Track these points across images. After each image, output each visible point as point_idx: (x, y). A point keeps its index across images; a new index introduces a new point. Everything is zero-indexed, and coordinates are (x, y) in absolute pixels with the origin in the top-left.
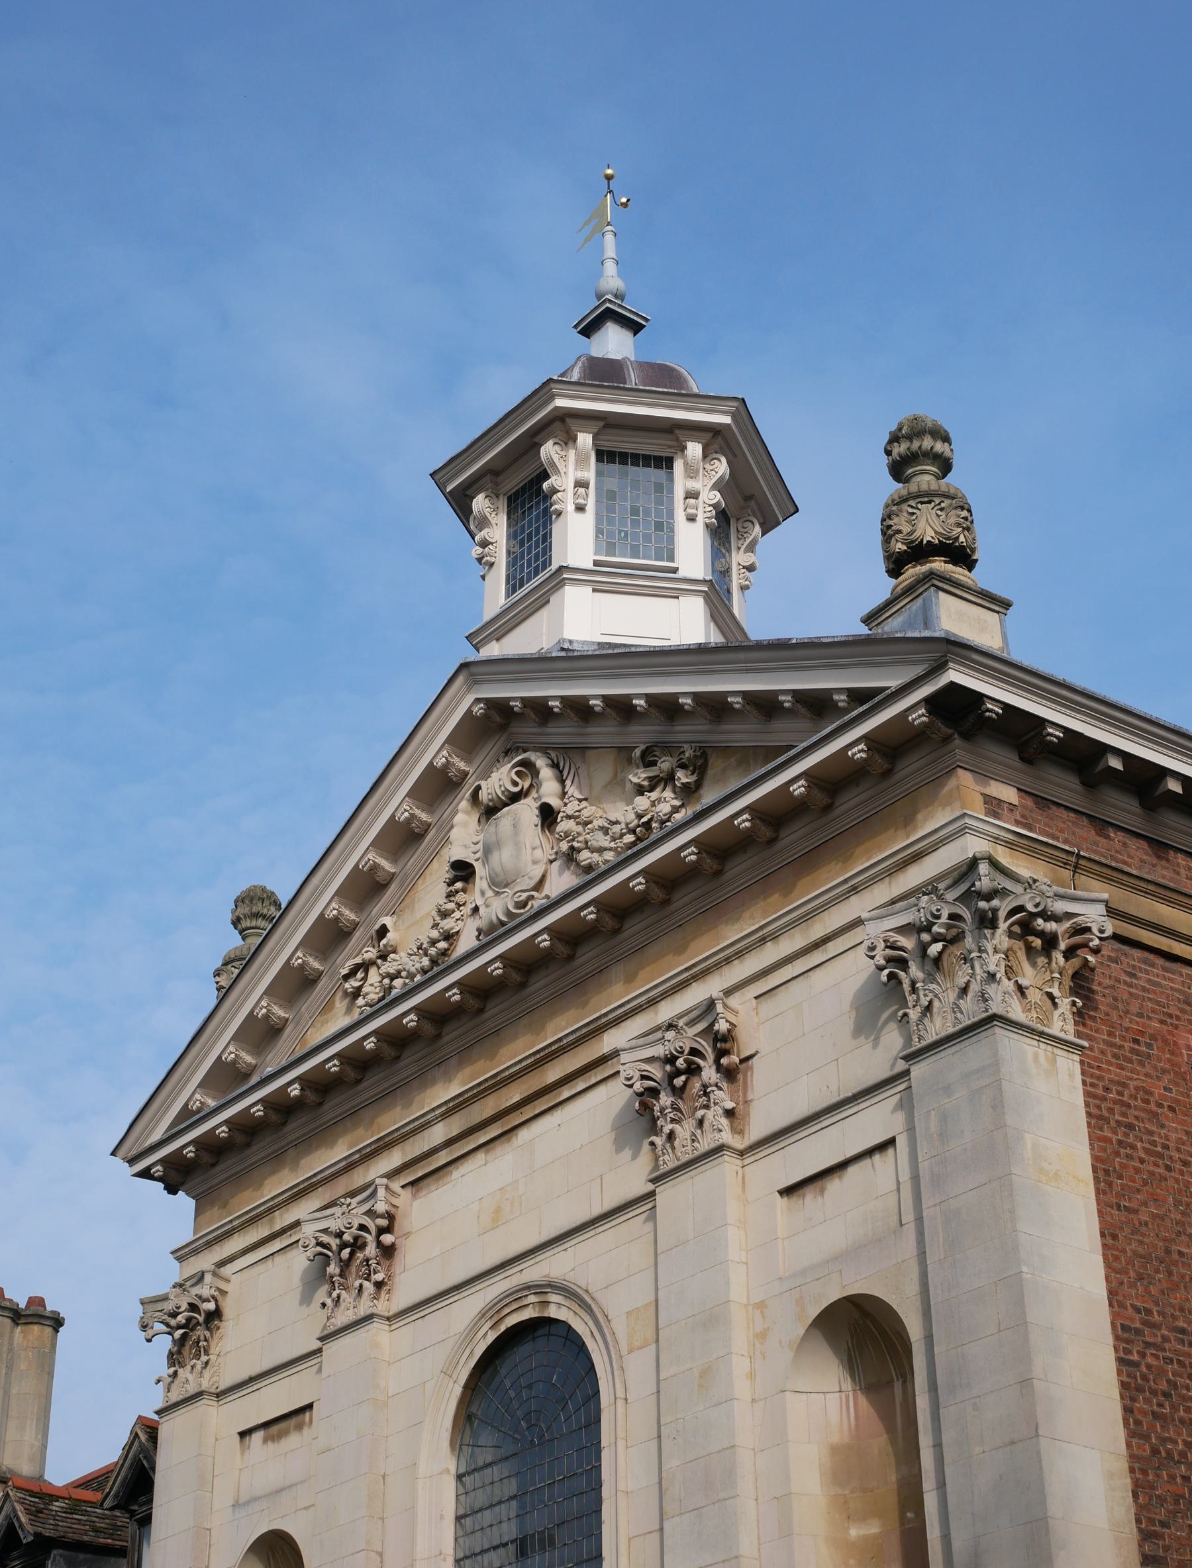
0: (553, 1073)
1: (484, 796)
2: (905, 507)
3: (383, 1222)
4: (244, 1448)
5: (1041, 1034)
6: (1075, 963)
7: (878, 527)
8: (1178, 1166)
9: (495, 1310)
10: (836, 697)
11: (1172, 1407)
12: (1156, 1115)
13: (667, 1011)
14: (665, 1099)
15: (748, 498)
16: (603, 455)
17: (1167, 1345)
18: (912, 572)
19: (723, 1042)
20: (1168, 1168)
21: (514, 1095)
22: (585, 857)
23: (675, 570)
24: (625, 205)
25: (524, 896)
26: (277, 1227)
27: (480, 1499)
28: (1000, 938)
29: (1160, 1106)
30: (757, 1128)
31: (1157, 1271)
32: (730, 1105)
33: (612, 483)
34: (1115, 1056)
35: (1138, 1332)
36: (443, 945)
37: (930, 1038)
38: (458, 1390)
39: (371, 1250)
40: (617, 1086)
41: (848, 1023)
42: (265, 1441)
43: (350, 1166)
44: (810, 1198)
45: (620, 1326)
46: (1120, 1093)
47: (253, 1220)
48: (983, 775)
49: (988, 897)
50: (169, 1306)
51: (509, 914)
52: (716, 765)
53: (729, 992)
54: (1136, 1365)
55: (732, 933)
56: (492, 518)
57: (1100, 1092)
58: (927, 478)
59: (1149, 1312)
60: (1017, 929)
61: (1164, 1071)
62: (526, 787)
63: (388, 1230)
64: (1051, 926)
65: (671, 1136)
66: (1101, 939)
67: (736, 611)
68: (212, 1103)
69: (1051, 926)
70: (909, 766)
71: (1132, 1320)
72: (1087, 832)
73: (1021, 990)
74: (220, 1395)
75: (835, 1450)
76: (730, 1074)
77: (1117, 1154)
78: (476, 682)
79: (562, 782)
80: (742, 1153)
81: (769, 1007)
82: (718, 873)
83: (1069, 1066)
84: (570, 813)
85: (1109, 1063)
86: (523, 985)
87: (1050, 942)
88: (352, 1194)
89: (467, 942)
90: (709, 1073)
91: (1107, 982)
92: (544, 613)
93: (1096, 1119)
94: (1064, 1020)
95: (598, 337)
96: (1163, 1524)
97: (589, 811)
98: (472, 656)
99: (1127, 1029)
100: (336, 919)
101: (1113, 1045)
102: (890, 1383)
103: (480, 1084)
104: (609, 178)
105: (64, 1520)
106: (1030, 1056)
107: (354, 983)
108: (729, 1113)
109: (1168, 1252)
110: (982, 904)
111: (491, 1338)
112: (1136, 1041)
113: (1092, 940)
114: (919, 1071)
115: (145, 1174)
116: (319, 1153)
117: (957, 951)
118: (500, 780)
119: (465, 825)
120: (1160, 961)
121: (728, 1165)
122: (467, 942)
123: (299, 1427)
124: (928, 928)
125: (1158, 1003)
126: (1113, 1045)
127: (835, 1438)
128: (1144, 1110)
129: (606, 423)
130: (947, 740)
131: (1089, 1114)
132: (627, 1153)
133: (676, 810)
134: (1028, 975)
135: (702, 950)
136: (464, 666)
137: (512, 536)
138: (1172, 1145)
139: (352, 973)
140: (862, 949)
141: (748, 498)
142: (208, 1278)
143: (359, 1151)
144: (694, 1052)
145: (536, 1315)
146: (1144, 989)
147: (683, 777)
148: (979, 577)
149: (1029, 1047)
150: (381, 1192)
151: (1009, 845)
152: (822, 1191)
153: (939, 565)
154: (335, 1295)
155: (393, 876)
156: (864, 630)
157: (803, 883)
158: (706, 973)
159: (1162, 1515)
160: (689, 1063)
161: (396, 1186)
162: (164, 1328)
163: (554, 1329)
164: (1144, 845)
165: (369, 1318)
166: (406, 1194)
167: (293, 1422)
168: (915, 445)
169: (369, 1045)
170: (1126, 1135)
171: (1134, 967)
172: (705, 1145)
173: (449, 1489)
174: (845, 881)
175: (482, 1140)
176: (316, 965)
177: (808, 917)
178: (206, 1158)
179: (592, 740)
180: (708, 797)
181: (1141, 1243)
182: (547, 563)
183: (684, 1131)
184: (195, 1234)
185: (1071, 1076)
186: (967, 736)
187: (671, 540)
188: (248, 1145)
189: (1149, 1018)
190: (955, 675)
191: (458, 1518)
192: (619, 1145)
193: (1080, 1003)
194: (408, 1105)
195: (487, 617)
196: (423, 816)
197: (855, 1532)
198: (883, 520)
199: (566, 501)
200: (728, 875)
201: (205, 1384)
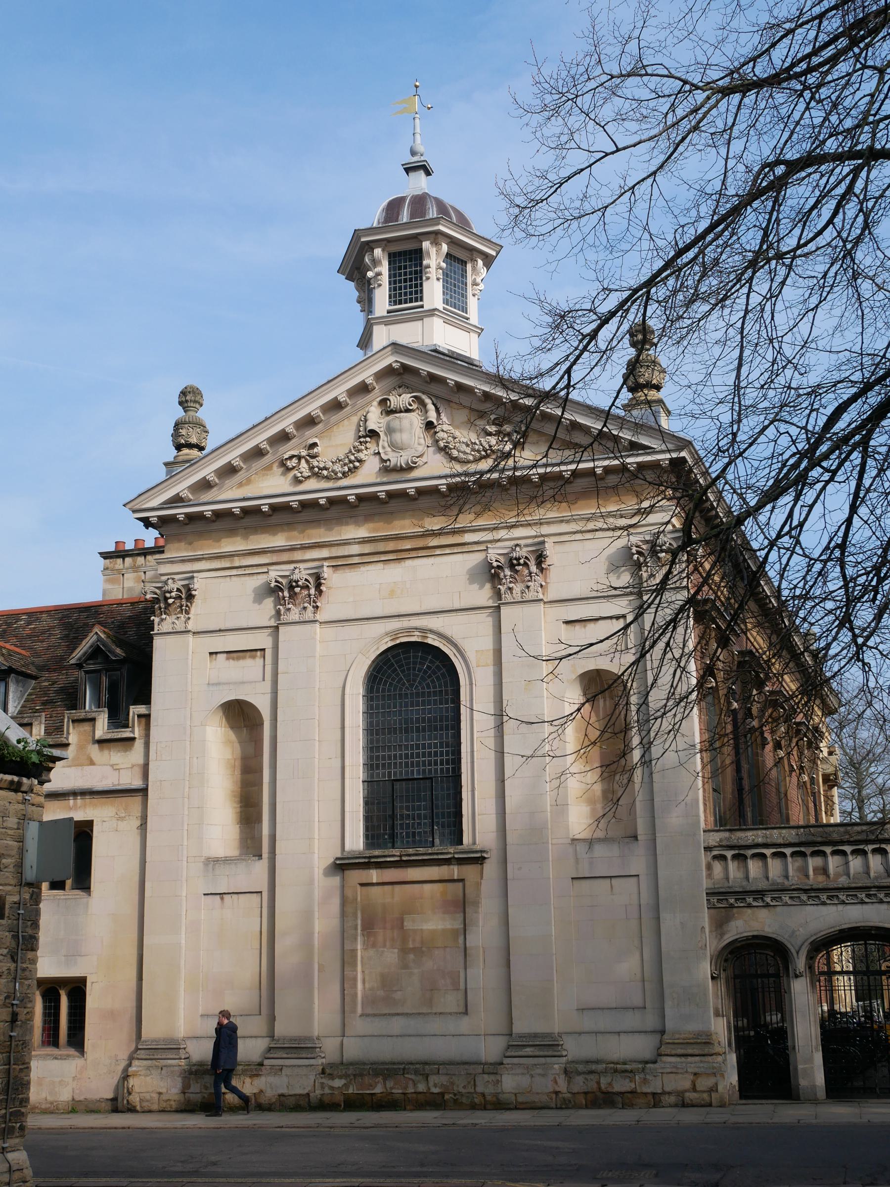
9: (395, 634)
19: (540, 558)
23: (468, 319)
78: (397, 352)
81: (559, 548)
116: (263, 536)
129: (453, 242)
145: (419, 640)
147: (515, 437)
152: (585, 627)
167: (248, 654)
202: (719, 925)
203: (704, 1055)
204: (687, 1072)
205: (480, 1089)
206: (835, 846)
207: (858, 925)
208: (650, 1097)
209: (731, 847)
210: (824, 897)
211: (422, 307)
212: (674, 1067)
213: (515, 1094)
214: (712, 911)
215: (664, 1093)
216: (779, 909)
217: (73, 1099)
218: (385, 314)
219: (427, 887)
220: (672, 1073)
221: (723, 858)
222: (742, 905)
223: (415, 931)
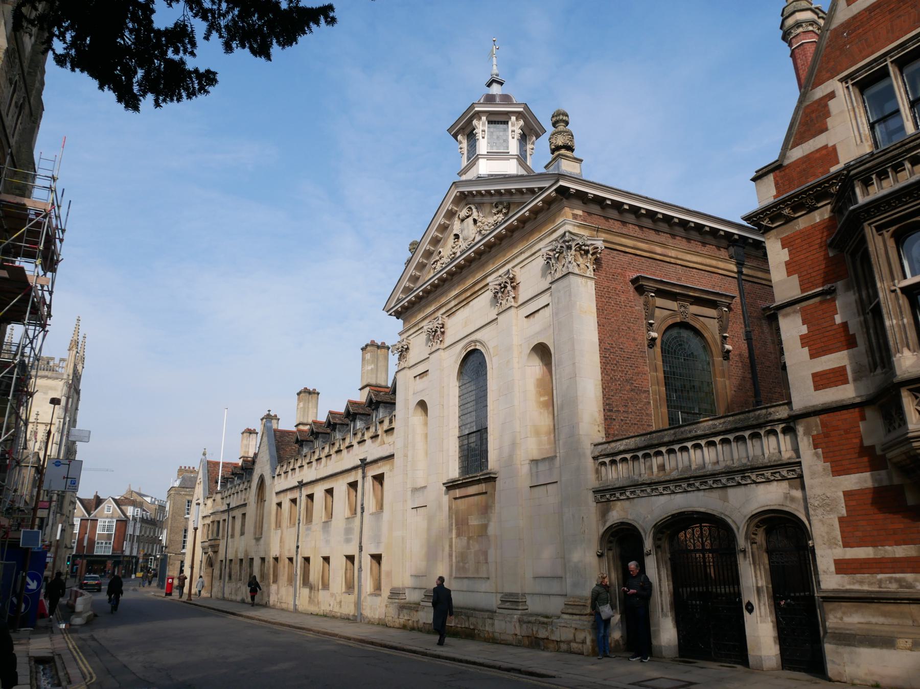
0: (477, 288)
1: (460, 217)
3: (441, 326)
4: (415, 380)
6: (595, 256)
9: (465, 347)
11: (617, 367)
12: (618, 294)
13: (501, 272)
14: (500, 294)
15: (532, 130)
16: (490, 122)
18: (556, 153)
19: (512, 280)
20: (620, 308)
21: (468, 294)
22: (483, 232)
23: (508, 153)
24: (498, 49)
27: (465, 391)
28: (573, 252)
30: (520, 302)
32: (514, 296)
33: (492, 130)
35: (608, 349)
36: (453, 256)
37: (556, 278)
38: (458, 366)
39: (439, 333)
41: (540, 275)
42: (420, 378)
43: (434, 312)
44: (531, 318)
45: (491, 350)
47: (415, 326)
48: (572, 208)
49: (568, 242)
50: (397, 347)
51: (467, 248)
53: (514, 267)
55: (515, 251)
56: (463, 141)
58: (562, 127)
59: (612, 344)
60: (578, 249)
61: (621, 282)
63: (443, 327)
64: (587, 248)
65: (501, 304)
67: (528, 164)
68: (404, 297)
69: (587, 248)
70: (554, 207)
72: (603, 221)
73: (578, 265)
74: (409, 368)
75: (538, 380)
76: (514, 288)
77: (606, 305)
79: (478, 212)
80: (517, 308)
81: (524, 270)
82: (512, 236)
83: (591, 285)
86: (470, 266)
87: (587, 252)
88: (434, 319)
89: (458, 254)
90: (509, 288)
92: (475, 166)
95: (491, 87)
96: (612, 396)
97: (484, 220)
98: (457, 179)
100: (429, 250)
104: (494, 41)
106: (580, 282)
107: (434, 266)
108: (514, 298)
109: (619, 329)
110: (567, 244)
112: (613, 275)
114: (553, 286)
115: (390, 315)
117: (562, 255)
118: (464, 213)
119: (457, 224)
120: (622, 254)
121: (513, 311)
123: (426, 375)
124: (555, 250)
129: (490, 113)
130: (562, 199)
132: (493, 308)
133: (503, 219)
134: (581, 261)
135: (509, 256)
136: (454, 183)
137: (468, 145)
140: (541, 257)
141: (532, 130)
142: (405, 340)
144: (506, 282)
147: (504, 211)
148: (576, 154)
149: (579, 279)
150: (440, 318)
153: (563, 151)
155: (442, 238)
156: (544, 171)
157: (531, 238)
159: (612, 393)
160: (505, 285)
161: (444, 317)
164: (619, 223)
165: (439, 349)
166: (447, 318)
168: (558, 118)
169: (436, 282)
172: (508, 306)
173: (457, 389)
176: (425, 261)
177: (531, 247)
178: (404, 310)
179: (485, 201)
180: (510, 215)
182: (475, 153)
183: (504, 302)
185: (592, 286)
186: (567, 199)
188: (413, 307)
190: (562, 183)
191: (459, 397)
192: (491, 305)
194: (447, 297)
195: (462, 168)
196: (448, 222)
197: (542, 399)
199: (479, 136)
200: (514, 236)
201: (406, 366)
202: (604, 514)
203: (582, 615)
204: (571, 627)
207: (683, 510)
209: (607, 455)
210: (661, 489)
212: (566, 623)
214: (599, 505)
215: (561, 641)
216: (636, 500)
218: (486, 153)
220: (564, 627)
221: (604, 464)
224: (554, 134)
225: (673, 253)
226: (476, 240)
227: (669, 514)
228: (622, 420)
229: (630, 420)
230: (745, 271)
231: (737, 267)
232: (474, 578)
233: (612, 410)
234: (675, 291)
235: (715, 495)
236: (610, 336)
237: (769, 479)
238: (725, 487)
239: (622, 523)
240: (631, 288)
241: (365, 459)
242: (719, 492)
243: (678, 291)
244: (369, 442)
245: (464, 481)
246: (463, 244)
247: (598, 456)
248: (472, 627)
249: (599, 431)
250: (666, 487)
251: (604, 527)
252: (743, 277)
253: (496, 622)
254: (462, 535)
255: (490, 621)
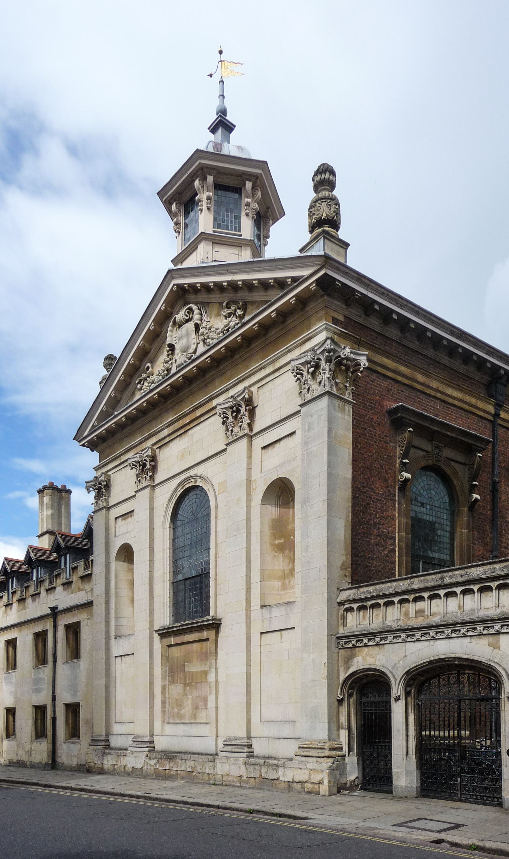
0: (198, 413)
2: (317, 204)
5: (341, 398)
7: (307, 212)
8: (378, 441)
10: (288, 280)
17: (367, 493)
19: (249, 402)
20: (375, 442)
21: (187, 420)
25: (190, 355)
26: (122, 461)
29: (376, 423)
31: (367, 472)
34: (364, 407)
35: (359, 488)
40: (216, 417)
42: (122, 520)
46: (364, 419)
52: (250, 308)
54: (358, 497)
57: (358, 418)
59: (363, 483)
62: (190, 317)
66: (363, 368)
71: (358, 485)
83: (349, 409)
84: (204, 326)
85: (361, 409)
87: (348, 368)
91: (364, 383)
93: (355, 426)
94: (349, 394)
99: (369, 398)
101: (363, 403)
102: (289, 503)
103: (177, 417)
105: (73, 542)
111: (181, 491)
112: (371, 403)
113: (361, 368)
114: (304, 410)
115: (83, 445)
122: (173, 371)
123: (131, 516)
125: (379, 391)
126: (363, 403)
127: (273, 517)
128: (370, 424)
131: (353, 424)
138: (377, 435)
139: (139, 382)
143: (144, 438)
146: (376, 386)
147: (239, 312)
151: (339, 335)
152: (274, 447)
154: (138, 479)
156: (298, 254)
158: (244, 380)
162: (92, 489)
163: (199, 488)
166: (157, 451)
170: (364, 431)
171: (373, 379)
174: (287, 348)
175: (179, 434)
180: (247, 318)
181: (364, 463)
184: (100, 462)
185: (349, 411)
187: (240, 223)
189: (376, 396)
193: (354, 389)
198: (309, 209)
205: (207, 771)
206: (431, 591)
207: (443, 657)
208: (287, 783)
210: (418, 635)
211: (241, 236)
213: (222, 775)
215: (293, 782)
217: (77, 764)
219: (195, 645)
222: (361, 645)
223: (189, 672)
224: (316, 201)
225: (434, 384)
226: (198, 353)
227: (427, 660)
228: (366, 566)
229: (374, 567)
230: (503, 415)
231: (495, 409)
232: (191, 723)
233: (358, 555)
234: (433, 428)
235: (484, 642)
236: (362, 473)
237: (481, 632)
238: (498, 633)
239: (369, 669)
240: (387, 420)
241: (56, 608)
242: (490, 639)
243: (436, 429)
244: (59, 589)
245: (181, 628)
246: (180, 358)
247: (345, 601)
248: (189, 770)
249: (346, 576)
250: (425, 634)
251: (346, 673)
252: (500, 422)
253: (218, 765)
254: (177, 683)
255: (212, 764)
